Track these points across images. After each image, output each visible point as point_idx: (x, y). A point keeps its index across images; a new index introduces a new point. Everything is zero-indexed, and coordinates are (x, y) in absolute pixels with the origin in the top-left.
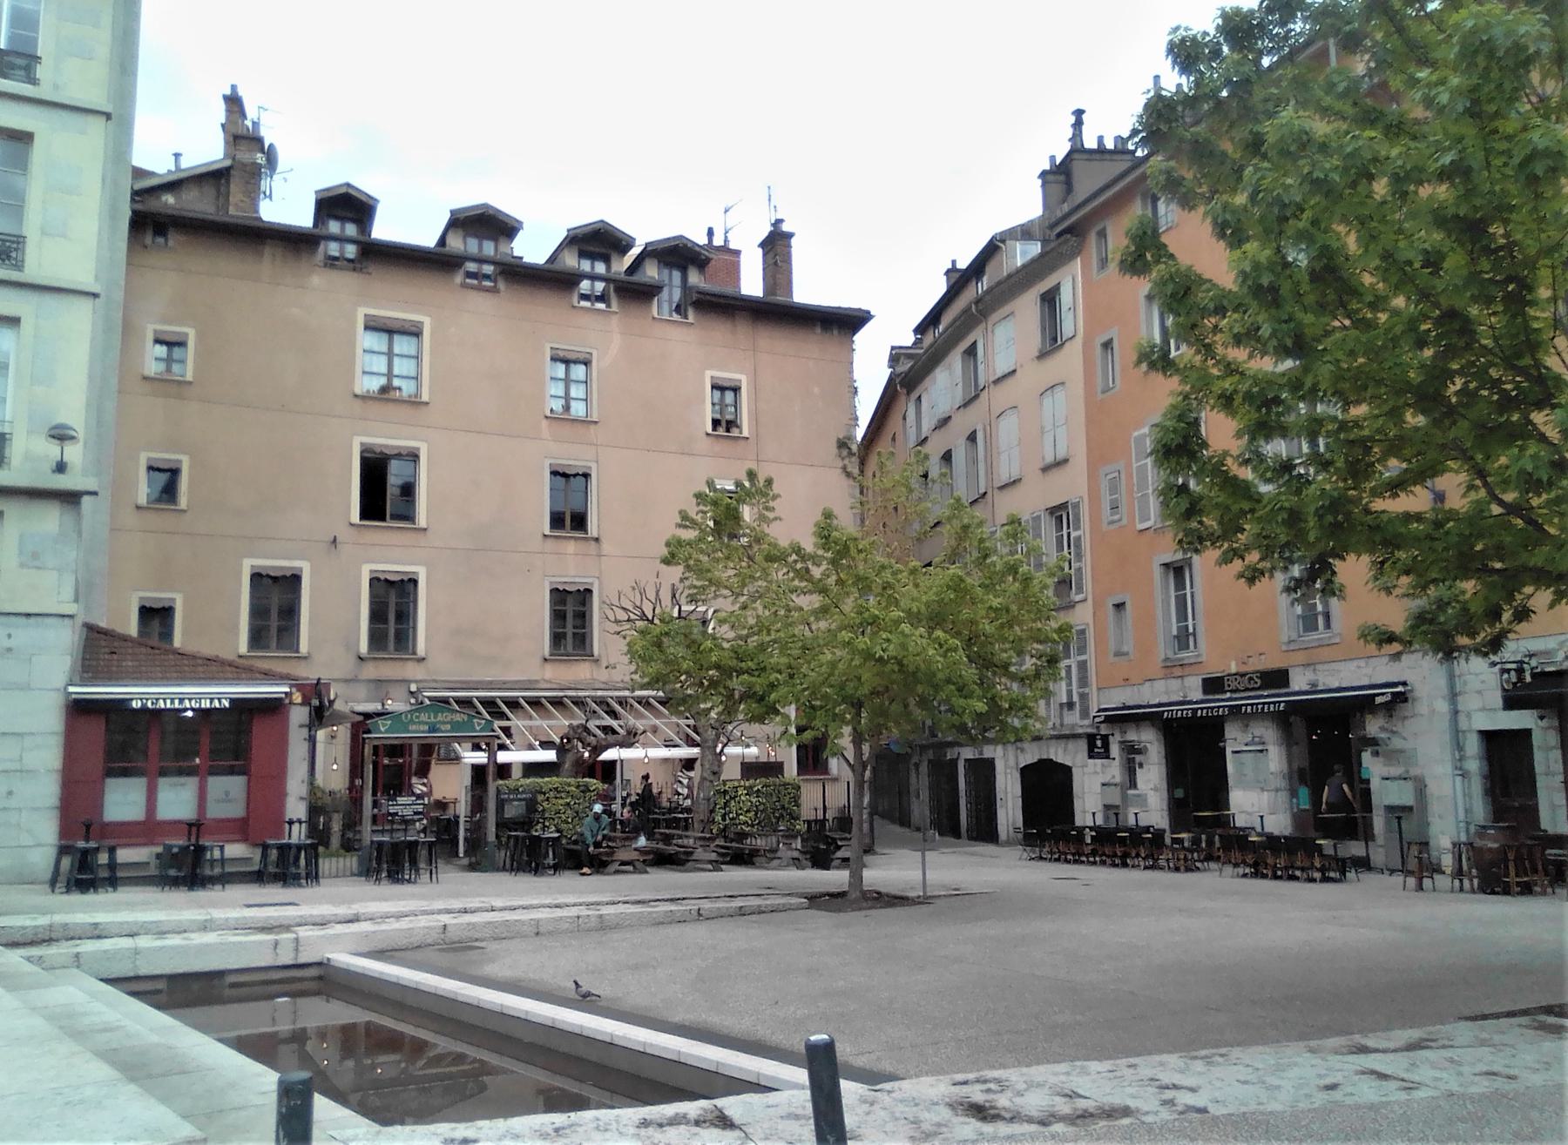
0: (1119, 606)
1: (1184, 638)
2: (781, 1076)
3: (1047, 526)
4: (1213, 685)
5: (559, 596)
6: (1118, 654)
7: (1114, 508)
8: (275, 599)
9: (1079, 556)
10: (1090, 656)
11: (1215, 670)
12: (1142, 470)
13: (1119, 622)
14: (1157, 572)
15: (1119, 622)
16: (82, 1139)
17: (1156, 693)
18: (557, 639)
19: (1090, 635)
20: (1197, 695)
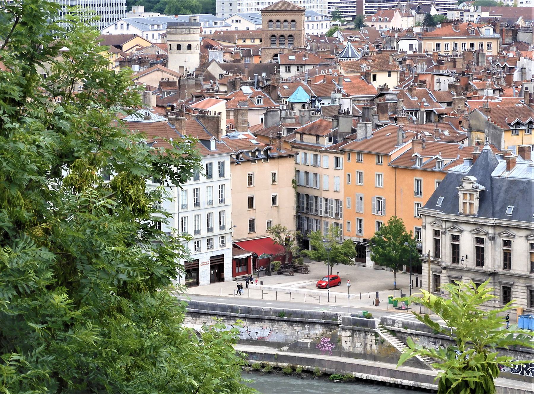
0: (349, 223)
1: (360, 231)
2: (525, 383)
3: (334, 202)
4: (364, 240)
5: (180, 49)
6: (348, 231)
7: (349, 205)
8: (251, 223)
9: (341, 211)
10: (342, 229)
11: (365, 238)
12: (374, 206)
13: (349, 226)
14: (356, 220)
15: (349, 226)
16: (286, 2)
17: (355, 239)
18: (510, 254)
19: (343, 226)
20: (362, 241)
